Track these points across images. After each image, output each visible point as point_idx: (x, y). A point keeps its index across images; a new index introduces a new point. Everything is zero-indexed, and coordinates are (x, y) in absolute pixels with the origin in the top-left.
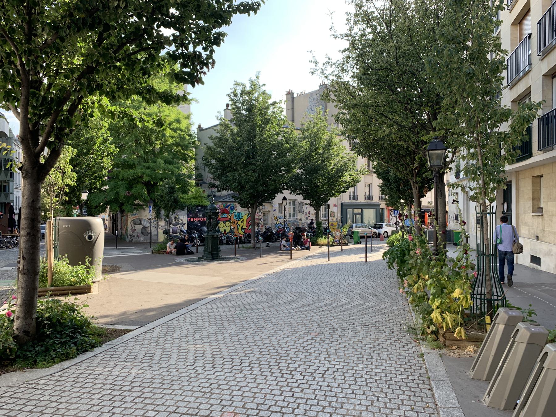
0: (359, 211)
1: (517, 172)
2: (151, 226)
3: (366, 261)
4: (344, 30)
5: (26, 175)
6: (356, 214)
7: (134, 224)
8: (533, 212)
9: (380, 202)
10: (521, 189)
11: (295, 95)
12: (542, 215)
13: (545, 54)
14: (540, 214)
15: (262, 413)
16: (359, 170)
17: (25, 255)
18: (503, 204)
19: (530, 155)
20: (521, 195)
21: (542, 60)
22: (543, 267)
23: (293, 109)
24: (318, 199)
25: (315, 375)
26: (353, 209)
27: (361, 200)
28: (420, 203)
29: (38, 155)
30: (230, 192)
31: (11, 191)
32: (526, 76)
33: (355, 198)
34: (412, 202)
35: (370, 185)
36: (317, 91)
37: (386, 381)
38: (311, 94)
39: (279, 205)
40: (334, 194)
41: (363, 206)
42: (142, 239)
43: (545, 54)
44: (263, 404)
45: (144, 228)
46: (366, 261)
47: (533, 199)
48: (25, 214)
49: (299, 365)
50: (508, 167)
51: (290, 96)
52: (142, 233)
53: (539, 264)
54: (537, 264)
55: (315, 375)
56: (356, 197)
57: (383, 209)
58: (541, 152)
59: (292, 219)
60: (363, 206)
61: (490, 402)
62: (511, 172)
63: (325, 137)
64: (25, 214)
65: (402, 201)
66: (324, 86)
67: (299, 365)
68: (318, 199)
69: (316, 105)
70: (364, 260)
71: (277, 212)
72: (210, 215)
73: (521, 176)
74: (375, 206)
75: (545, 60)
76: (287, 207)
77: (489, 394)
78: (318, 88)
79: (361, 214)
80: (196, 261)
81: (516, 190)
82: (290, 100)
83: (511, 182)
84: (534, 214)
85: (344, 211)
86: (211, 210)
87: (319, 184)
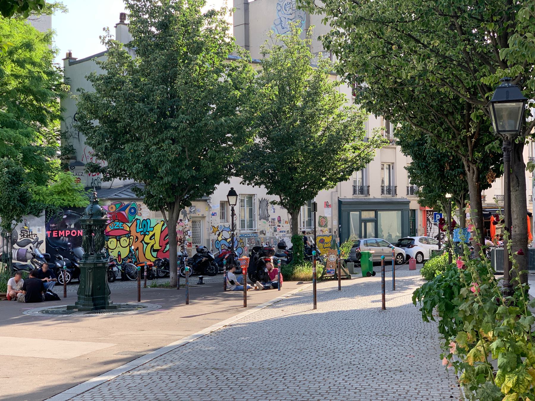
0: (372, 214)
3: (384, 307)
6: (366, 221)
16: (371, 138)
23: (246, 24)
24: (295, 193)
27: (375, 194)
28: (479, 199)
33: (363, 190)
41: (378, 206)
46: (384, 307)
59: (247, 231)
60: (378, 206)
65: (448, 196)
68: (295, 193)
69: (291, 17)
71: (217, 218)
72: (90, 226)
76: (236, 209)
79: (375, 221)
80: (64, 313)
85: (344, 214)
86: (92, 215)
87: (296, 165)
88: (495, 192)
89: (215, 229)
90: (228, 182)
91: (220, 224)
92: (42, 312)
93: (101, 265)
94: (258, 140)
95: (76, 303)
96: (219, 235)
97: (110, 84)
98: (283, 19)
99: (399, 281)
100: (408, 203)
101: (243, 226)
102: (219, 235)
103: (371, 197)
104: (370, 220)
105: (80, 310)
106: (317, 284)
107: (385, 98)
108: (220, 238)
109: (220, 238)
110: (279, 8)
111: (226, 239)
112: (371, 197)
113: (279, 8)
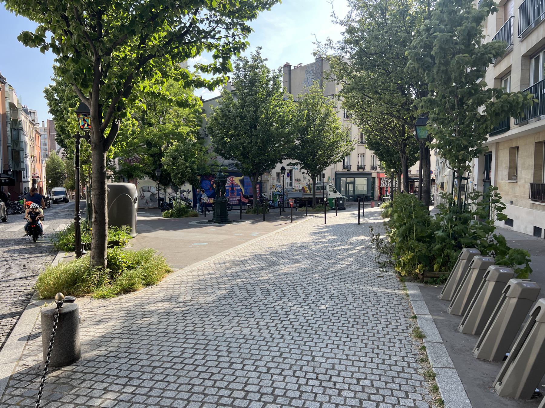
0: (352, 179)
1: (497, 144)
2: (159, 193)
3: (359, 223)
4: (342, 17)
5: (95, 146)
6: (349, 183)
7: (143, 191)
8: (509, 180)
9: (372, 171)
10: (500, 159)
11: (292, 68)
12: (362, 143)
13: (525, 35)
14: (515, 181)
15: (237, 403)
16: (352, 140)
17: (97, 210)
18: (484, 173)
19: (508, 129)
20: (499, 164)
21: (522, 42)
22: (515, 228)
23: (290, 81)
24: (314, 168)
25: (324, 297)
26: (346, 178)
27: (354, 169)
28: (407, 172)
29: (103, 130)
30: (231, 161)
31: (22, 160)
32: (508, 56)
33: (349, 168)
34: (401, 171)
35: (363, 155)
36: (313, 64)
37: (377, 301)
38: (307, 67)
39: (278, 174)
40: (329, 164)
41: (355, 175)
42: (151, 205)
43: (525, 35)
44: (260, 360)
45: (153, 194)
46: (359, 223)
47: (510, 168)
48: (95, 177)
49: (312, 292)
50: (490, 139)
51: (287, 69)
52: (151, 199)
53: (512, 226)
54: (510, 225)
55: (324, 297)
56: (349, 167)
57: (374, 178)
58: (517, 126)
59: (289, 187)
60: (355, 175)
61: (452, 311)
62: (492, 143)
63: (323, 111)
64: (95, 177)
65: (392, 170)
66: (320, 59)
67: (312, 292)
68: (314, 168)
69: (313, 77)
70: (357, 222)
71: (275, 181)
72: (219, 183)
73: (500, 147)
74: (367, 175)
75: (525, 42)
76: (288, 176)
77: (451, 306)
78: (314, 61)
79: (354, 183)
80: (207, 223)
81: (496, 160)
82: (287, 72)
83: (491, 152)
84: (510, 181)
85: (338, 180)
86: (219, 178)
87: (314, 152)
88: (415, 169)
89: (274, 187)
90: (281, 163)
92: (7, 252)
94: (297, 142)
97: (225, 113)
100: (371, 174)
101: (288, 185)
103: (352, 171)
104: (351, 183)
105: (215, 222)
107: (384, 218)
112: (352, 171)
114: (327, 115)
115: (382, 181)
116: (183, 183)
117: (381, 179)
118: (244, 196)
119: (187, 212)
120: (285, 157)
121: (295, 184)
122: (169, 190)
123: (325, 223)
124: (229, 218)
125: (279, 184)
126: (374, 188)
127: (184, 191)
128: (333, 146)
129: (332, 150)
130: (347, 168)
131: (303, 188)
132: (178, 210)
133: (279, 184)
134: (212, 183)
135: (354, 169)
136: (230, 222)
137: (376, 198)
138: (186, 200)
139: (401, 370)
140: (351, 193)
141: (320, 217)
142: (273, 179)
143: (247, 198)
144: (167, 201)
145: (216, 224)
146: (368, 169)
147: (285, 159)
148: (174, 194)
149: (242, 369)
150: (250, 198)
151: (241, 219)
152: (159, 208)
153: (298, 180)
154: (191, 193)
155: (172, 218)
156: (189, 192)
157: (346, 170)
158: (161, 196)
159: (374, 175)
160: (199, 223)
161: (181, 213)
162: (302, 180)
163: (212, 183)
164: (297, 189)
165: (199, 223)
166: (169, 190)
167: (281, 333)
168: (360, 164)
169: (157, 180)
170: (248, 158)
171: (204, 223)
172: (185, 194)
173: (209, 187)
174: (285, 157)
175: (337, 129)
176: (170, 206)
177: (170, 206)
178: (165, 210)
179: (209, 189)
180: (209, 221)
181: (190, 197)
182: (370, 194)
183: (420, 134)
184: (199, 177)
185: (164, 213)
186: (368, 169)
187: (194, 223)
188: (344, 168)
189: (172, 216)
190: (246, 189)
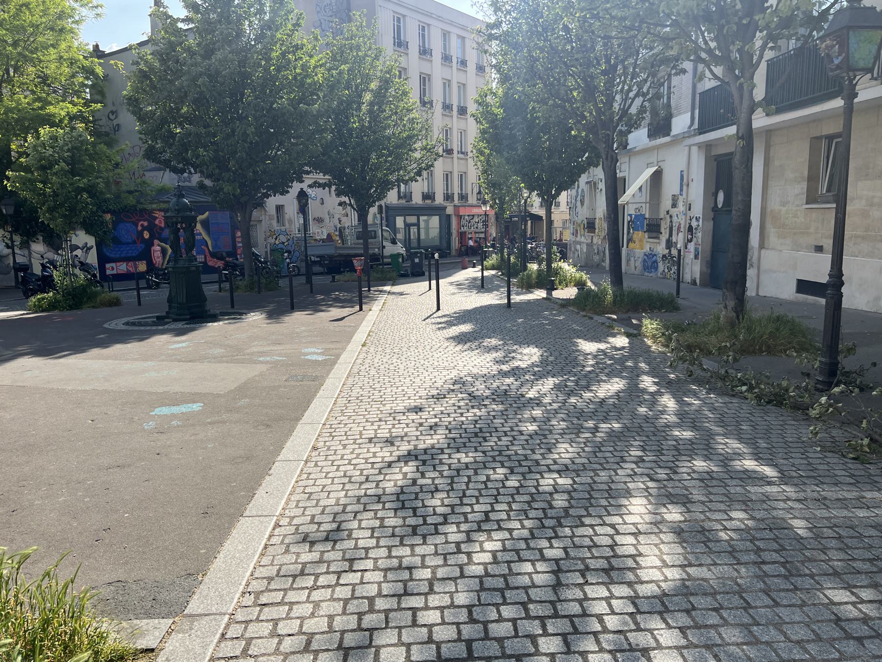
9: (446, 204)
27: (417, 199)
33: (408, 196)
71: (274, 222)
74: (439, 211)
79: (418, 225)
80: (154, 324)
86: (178, 211)
89: (272, 233)
91: (276, 228)
92: (127, 324)
93: (194, 268)
95: (167, 313)
96: (276, 239)
98: (322, 21)
99: (145, 295)
102: (276, 239)
103: (414, 202)
104: (413, 225)
105: (175, 320)
106: (440, 281)
108: (277, 242)
109: (277, 242)
110: (318, 9)
111: (283, 243)
112: (414, 202)
113: (318, 9)
114: (386, 83)
115: (463, 222)
116: (71, 226)
117: (460, 217)
118: (213, 255)
119: (93, 296)
120: (307, 168)
121: (313, 229)
122: (38, 247)
123: (438, 309)
124: (207, 308)
125: (283, 228)
126: (449, 234)
127: (76, 247)
128: (406, 144)
129: (399, 157)
130: (405, 196)
131: (329, 235)
132: (69, 294)
133: (283, 228)
134: (140, 228)
135: (417, 199)
136: (214, 318)
137: (454, 253)
138: (84, 267)
139: (490, 509)
140: (414, 244)
141: (401, 294)
142: (271, 218)
143: (221, 258)
144: (37, 270)
145: (173, 326)
146: (439, 200)
147: (308, 173)
148: (51, 255)
149: (276, 622)
150: (227, 259)
151: (234, 310)
152: (16, 287)
153: (319, 220)
154: (94, 252)
155: (56, 312)
156: (87, 249)
157: (403, 201)
158: (20, 260)
159: (450, 210)
160: (133, 324)
161: (76, 299)
162: (327, 220)
163: (140, 228)
164: (318, 238)
165: (133, 324)
166: (38, 247)
167: (322, 503)
168: (426, 190)
169: (6, 223)
170: (229, 170)
171: (146, 324)
172: (78, 252)
173: (135, 237)
174: (307, 168)
175: (409, 111)
176: (46, 283)
177: (46, 283)
178: (34, 293)
179: (134, 242)
180: (158, 318)
181: (92, 258)
182: (445, 244)
183: (857, 56)
184: (108, 217)
185: (33, 299)
186: (439, 200)
187: (118, 324)
188: (400, 197)
189: (53, 306)
190: (215, 240)
